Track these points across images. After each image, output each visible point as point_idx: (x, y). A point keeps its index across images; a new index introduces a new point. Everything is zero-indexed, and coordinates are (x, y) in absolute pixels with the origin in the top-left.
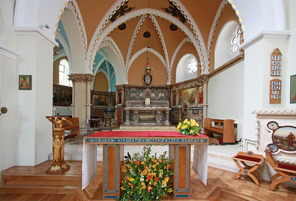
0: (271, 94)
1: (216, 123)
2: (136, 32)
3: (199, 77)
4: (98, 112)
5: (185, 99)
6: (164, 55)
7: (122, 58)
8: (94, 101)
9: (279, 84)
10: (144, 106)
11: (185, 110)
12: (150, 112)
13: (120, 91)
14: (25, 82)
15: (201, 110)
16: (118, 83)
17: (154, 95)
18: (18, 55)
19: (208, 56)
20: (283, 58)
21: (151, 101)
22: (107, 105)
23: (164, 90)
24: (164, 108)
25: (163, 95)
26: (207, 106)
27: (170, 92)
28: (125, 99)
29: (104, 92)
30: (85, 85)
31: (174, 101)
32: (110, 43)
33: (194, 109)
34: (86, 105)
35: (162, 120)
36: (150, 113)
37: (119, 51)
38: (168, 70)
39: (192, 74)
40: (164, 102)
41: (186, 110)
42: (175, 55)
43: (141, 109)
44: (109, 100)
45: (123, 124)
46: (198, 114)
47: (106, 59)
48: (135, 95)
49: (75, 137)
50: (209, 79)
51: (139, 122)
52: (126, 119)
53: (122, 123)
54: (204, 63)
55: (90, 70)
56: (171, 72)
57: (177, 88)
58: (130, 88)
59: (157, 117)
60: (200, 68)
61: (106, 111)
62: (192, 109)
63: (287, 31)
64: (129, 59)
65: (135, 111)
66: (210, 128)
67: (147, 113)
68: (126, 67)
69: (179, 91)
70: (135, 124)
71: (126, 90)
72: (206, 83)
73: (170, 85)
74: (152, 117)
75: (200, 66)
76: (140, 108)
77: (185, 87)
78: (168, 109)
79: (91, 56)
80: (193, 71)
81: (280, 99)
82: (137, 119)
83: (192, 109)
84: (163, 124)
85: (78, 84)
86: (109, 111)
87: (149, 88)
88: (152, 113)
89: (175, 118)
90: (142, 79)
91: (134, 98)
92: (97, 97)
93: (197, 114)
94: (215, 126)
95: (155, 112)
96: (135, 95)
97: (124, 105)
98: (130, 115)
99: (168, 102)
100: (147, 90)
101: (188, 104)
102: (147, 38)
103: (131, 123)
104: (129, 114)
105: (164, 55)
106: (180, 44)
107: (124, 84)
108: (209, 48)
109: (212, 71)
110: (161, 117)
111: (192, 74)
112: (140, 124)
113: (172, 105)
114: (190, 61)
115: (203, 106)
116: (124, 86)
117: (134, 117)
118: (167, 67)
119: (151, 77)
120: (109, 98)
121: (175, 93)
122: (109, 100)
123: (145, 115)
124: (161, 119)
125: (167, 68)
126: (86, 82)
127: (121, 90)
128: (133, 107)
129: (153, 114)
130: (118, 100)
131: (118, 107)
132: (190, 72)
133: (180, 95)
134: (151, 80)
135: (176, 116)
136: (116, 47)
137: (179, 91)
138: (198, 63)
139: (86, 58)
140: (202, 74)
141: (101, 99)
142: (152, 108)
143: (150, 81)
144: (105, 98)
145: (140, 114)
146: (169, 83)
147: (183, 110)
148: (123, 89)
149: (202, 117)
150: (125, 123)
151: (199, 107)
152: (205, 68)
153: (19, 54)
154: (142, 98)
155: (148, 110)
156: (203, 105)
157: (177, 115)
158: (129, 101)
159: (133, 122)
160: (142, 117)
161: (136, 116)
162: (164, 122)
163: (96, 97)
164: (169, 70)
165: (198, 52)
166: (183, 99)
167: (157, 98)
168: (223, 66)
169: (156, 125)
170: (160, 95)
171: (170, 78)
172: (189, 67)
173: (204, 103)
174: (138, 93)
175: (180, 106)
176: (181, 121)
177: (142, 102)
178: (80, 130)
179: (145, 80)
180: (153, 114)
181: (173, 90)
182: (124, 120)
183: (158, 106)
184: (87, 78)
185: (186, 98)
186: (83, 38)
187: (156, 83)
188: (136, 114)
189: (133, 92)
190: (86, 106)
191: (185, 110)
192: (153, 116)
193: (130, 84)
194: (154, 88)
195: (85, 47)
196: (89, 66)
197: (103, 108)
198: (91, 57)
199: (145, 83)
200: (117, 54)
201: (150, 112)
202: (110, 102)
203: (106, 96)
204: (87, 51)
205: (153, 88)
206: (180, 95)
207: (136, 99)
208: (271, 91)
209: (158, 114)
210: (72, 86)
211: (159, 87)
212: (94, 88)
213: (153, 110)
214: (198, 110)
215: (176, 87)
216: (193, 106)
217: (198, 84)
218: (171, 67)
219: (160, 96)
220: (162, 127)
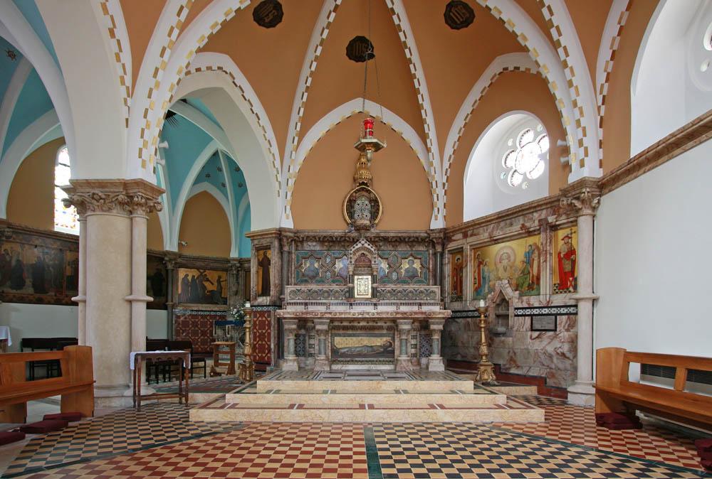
1: (646, 370)
2: (320, 33)
3: (561, 190)
4: (195, 324)
5: (500, 279)
7: (271, 134)
8: (183, 289)
10: (351, 305)
11: (498, 316)
12: (370, 326)
15: (564, 318)
16: (257, 226)
17: (384, 265)
19: (599, 108)
21: (375, 285)
22: (225, 303)
23: (422, 248)
24: (425, 308)
25: (417, 265)
26: (594, 301)
27: (442, 254)
28: (282, 280)
29: (216, 260)
30: (127, 221)
31: (458, 285)
32: (228, 77)
33: (536, 312)
34: (130, 297)
35: (414, 355)
36: (373, 328)
37: (258, 107)
38: (433, 177)
39: (524, 186)
40: (422, 288)
42: (459, 122)
43: (341, 313)
44: (231, 284)
45: (277, 365)
46: (555, 330)
47: (221, 147)
49: (70, 424)
50: (600, 196)
51: (333, 362)
52: (285, 349)
53: (273, 363)
54: (580, 136)
55: (144, 166)
56: (444, 184)
57: (470, 239)
58: (302, 242)
59: (397, 343)
60: (563, 160)
61: (221, 322)
62: (528, 312)
64: (296, 139)
65: (316, 320)
66: (621, 389)
68: (286, 169)
69: (475, 248)
70: (317, 368)
71: (286, 249)
72: (589, 211)
73: (441, 231)
74: (378, 342)
75: (566, 150)
76: (333, 308)
77: (498, 234)
78: (440, 313)
79: (146, 111)
80: (528, 176)
82: (322, 350)
83: (528, 312)
84: (418, 368)
85: (95, 219)
86: (231, 322)
87: (370, 241)
88: (381, 328)
89: (460, 344)
91: (313, 277)
92: (193, 276)
93: (551, 333)
94: (642, 379)
95: (389, 324)
96: (316, 265)
97: (280, 299)
98: (297, 336)
99: (437, 289)
100: (360, 245)
101: (510, 293)
102: (360, 63)
103: (302, 365)
104: (295, 333)
107: (278, 227)
108: (601, 77)
109: (616, 164)
110: (413, 342)
111: (524, 186)
112: (335, 367)
113: (447, 300)
114: (514, 142)
115: (578, 300)
116: (280, 234)
117: (312, 342)
118: (432, 165)
119: (374, 202)
120: (232, 280)
121: (459, 256)
122: (231, 284)
123: (354, 335)
124: (413, 351)
125: (432, 169)
126: (131, 212)
127: (268, 248)
128: (311, 308)
129: (385, 332)
130: (258, 285)
131: (254, 309)
132: (517, 180)
133: (480, 263)
134: (374, 214)
135: (465, 336)
136: (250, 93)
137: (475, 248)
138: (553, 142)
139: (127, 120)
140: (573, 178)
141: (206, 284)
142: (380, 309)
143: (369, 215)
144: (220, 277)
145: (334, 332)
146: (438, 223)
148: (276, 243)
149: (574, 342)
150: (281, 361)
151: (557, 307)
152: (586, 155)
155: (364, 319)
156: (577, 296)
157: (470, 333)
158: (295, 284)
159: (310, 361)
160: (342, 342)
161: (322, 337)
162: (424, 361)
163: (187, 275)
164: (439, 177)
165: (558, 96)
166: (492, 277)
167: (394, 276)
168: (683, 130)
169: (395, 371)
170: (407, 266)
171: (440, 204)
172: (510, 163)
173: (584, 291)
174: (328, 260)
175: (482, 304)
176: (486, 355)
177: (343, 287)
178: (96, 393)
179: (351, 215)
180: (385, 332)
181: (452, 246)
182: (280, 355)
184: (132, 197)
188: (322, 331)
189: (312, 255)
190: (130, 302)
191: (498, 316)
192: (385, 339)
193: (300, 228)
194: (386, 239)
195: (122, 79)
196: (141, 150)
197: (212, 313)
198: (145, 117)
199: (352, 224)
200: (252, 119)
201: (371, 324)
202: (236, 293)
203: (224, 275)
204: (130, 93)
205: (382, 241)
206: (480, 263)
207: (322, 281)
209: (400, 332)
210: (75, 230)
211: (404, 238)
212: (180, 245)
213: (384, 316)
214: (556, 315)
215: (465, 236)
216: (534, 301)
217: (551, 219)
218: (446, 165)
219: (407, 271)
220: (420, 382)
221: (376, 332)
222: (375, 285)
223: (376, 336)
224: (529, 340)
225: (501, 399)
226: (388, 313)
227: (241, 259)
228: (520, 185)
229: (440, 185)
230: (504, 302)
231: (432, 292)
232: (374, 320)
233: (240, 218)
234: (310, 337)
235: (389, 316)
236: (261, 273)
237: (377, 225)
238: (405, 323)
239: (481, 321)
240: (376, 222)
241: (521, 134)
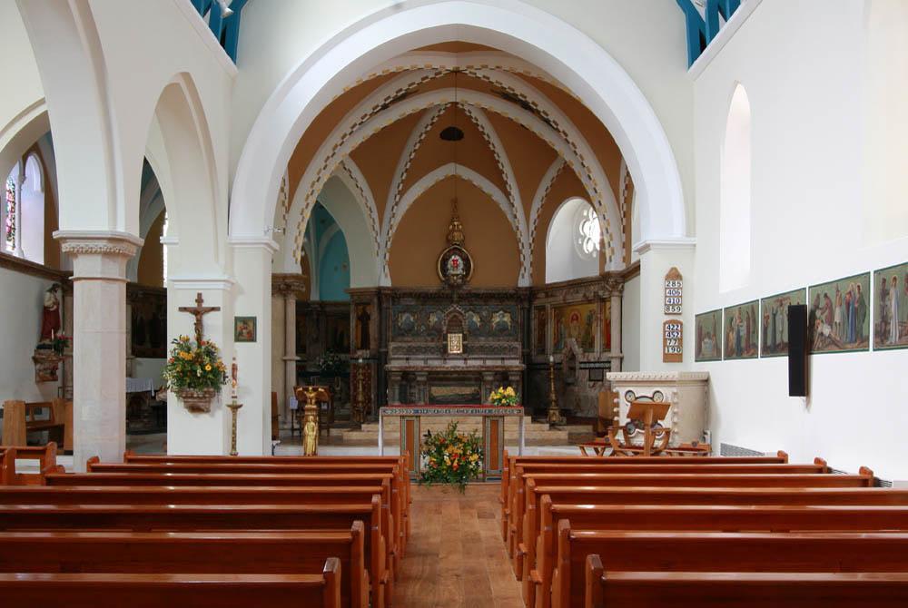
0: (665, 345)
6: (502, 185)
7: (372, 203)
9: (679, 328)
12: (461, 377)
13: (364, 309)
14: (246, 328)
18: (233, 284)
20: (685, 284)
21: (465, 342)
24: (508, 363)
25: (507, 319)
26: (622, 359)
27: (529, 311)
30: (283, 302)
33: (592, 365)
34: (284, 358)
39: (595, 255)
41: (573, 369)
48: (412, 319)
50: (624, 283)
53: (373, 412)
57: (550, 299)
59: (483, 392)
62: (587, 366)
63: (688, 239)
67: (454, 379)
71: (384, 305)
72: (617, 293)
73: (526, 289)
74: (468, 391)
76: (430, 362)
77: (570, 299)
78: (517, 367)
81: (681, 354)
83: (587, 366)
88: (470, 379)
90: (438, 275)
91: (409, 331)
93: (600, 383)
98: (401, 386)
101: (578, 350)
105: (502, 185)
106: (543, 181)
107: (377, 285)
114: (588, 214)
116: (379, 292)
117: (412, 391)
129: (473, 382)
130: (357, 338)
142: (470, 363)
145: (431, 382)
146: (524, 282)
147: (565, 369)
148: (376, 300)
151: (603, 362)
153: (234, 281)
154: (436, 330)
156: (610, 355)
160: (438, 391)
161: (422, 387)
164: (525, 239)
166: (567, 335)
170: (498, 320)
171: (527, 264)
173: (615, 351)
179: (444, 269)
180: (473, 382)
181: (537, 303)
183: (487, 359)
185: (575, 333)
186: (309, 201)
187: (484, 279)
189: (407, 310)
190: (285, 361)
192: (473, 389)
194: (477, 296)
201: (461, 375)
208: (665, 340)
215: (547, 296)
218: (532, 227)
219: (498, 324)
221: (466, 382)
222: (465, 342)
223: (467, 386)
224: (588, 389)
225: (563, 434)
226: (474, 367)
227: (323, 302)
228: (592, 253)
229: (526, 246)
230: (573, 357)
231: (516, 348)
232: (463, 372)
233: (320, 258)
234: (411, 387)
235: (475, 369)
236: (360, 326)
237: (469, 282)
238: (490, 375)
239: (549, 374)
240: (468, 279)
241: (582, 223)
